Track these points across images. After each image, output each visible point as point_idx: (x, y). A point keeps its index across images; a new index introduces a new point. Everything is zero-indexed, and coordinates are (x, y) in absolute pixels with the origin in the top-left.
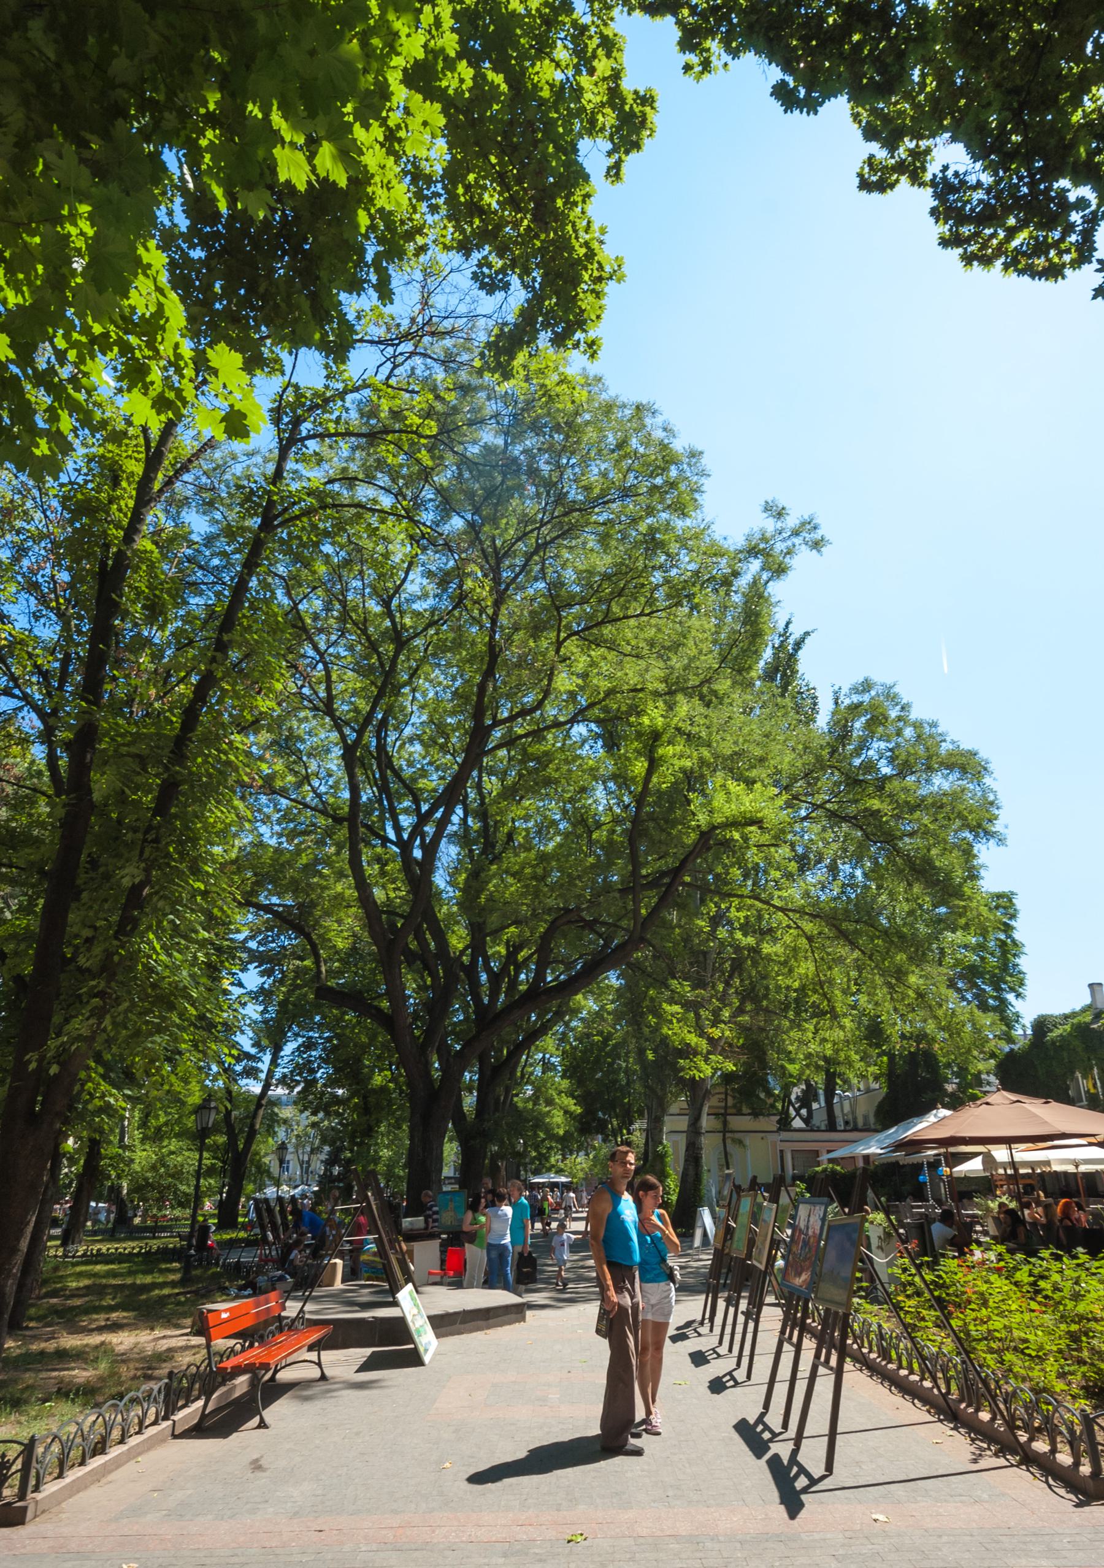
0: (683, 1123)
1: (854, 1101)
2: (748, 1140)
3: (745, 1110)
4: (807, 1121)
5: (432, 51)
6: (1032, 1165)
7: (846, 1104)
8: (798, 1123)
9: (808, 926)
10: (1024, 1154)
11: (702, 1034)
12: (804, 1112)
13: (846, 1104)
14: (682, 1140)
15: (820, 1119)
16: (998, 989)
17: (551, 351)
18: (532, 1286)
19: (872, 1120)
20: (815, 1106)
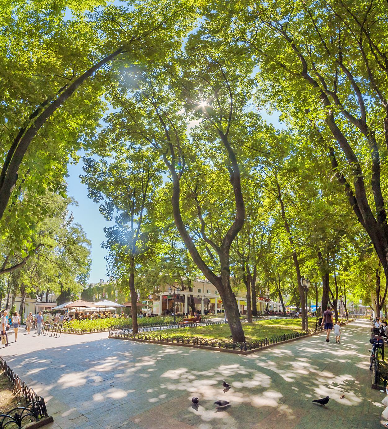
0: (20, 299)
1: (52, 296)
2: (29, 304)
3: (30, 297)
4: (41, 300)
5: (92, 195)
6: (83, 310)
7: (50, 297)
8: (39, 300)
9: (54, 265)
10: (81, 308)
11: (31, 283)
12: (40, 298)
13: (50, 297)
14: (19, 304)
15: (44, 300)
16: (85, 277)
17: (332, 332)
18: (301, 375)
19: (55, 300)
20: (43, 296)
